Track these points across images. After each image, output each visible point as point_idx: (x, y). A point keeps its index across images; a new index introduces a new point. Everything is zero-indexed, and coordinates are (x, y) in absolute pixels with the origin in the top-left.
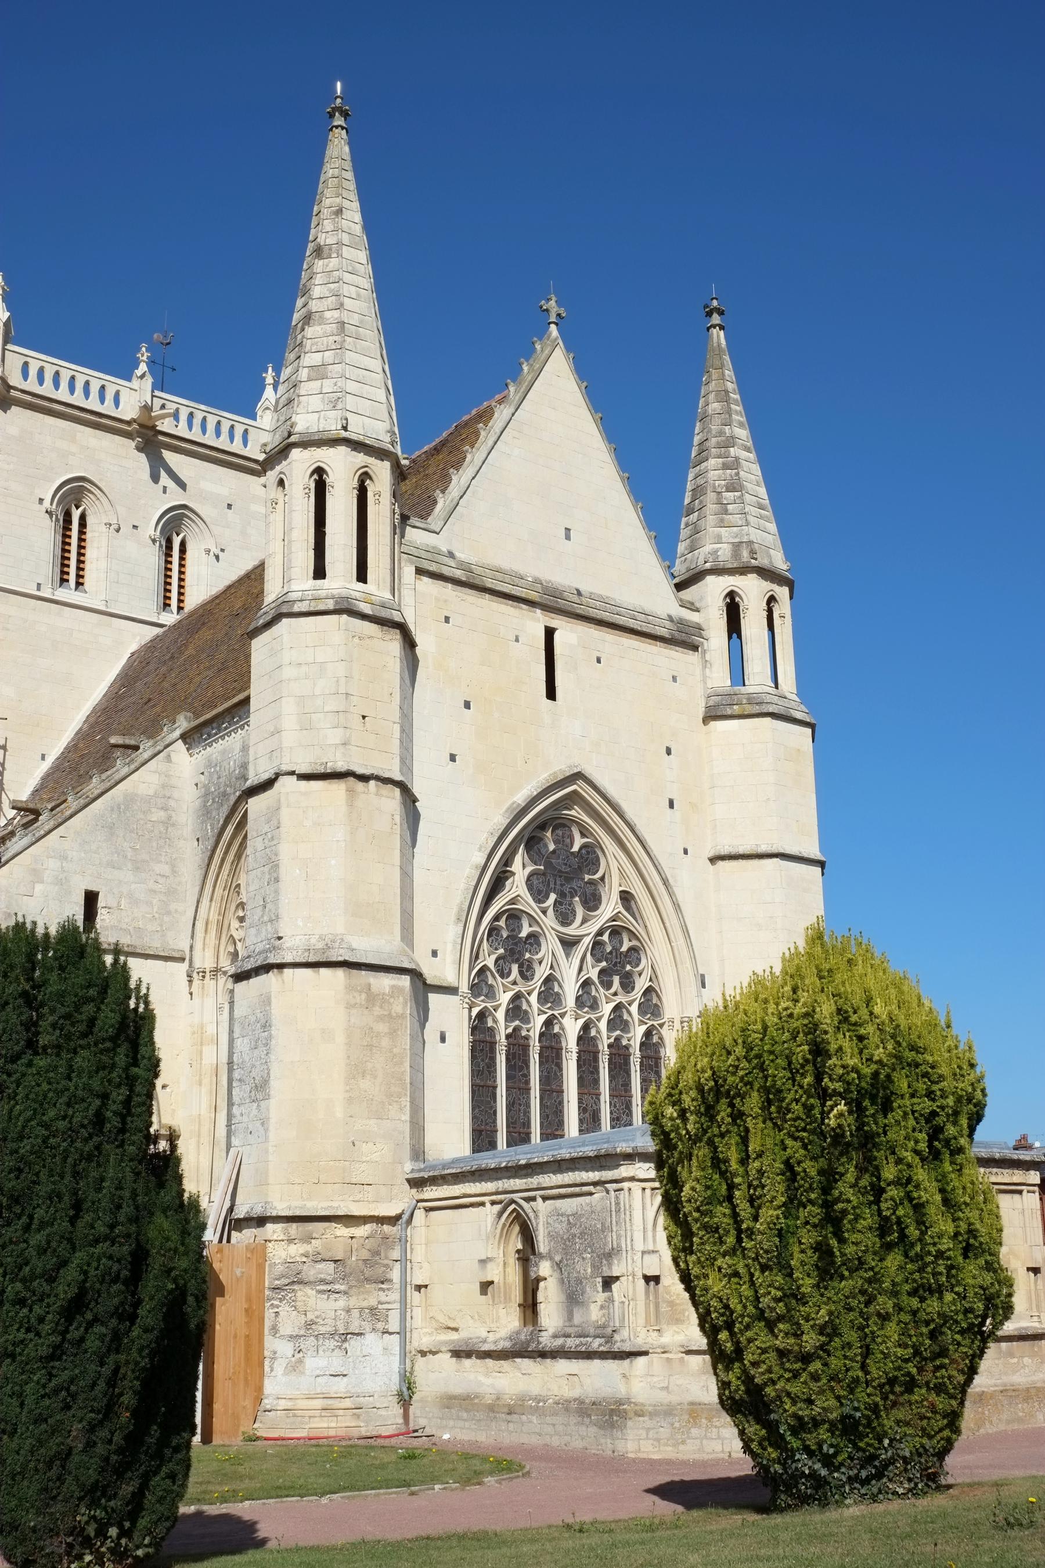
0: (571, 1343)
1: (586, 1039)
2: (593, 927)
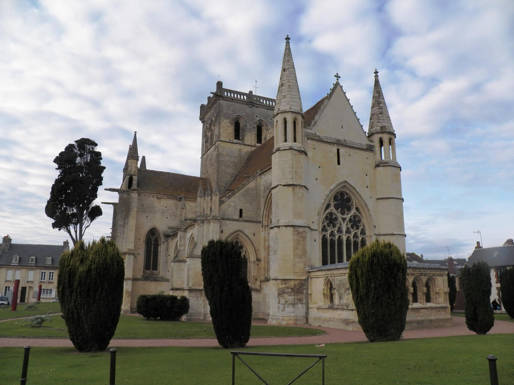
0: (340, 307)
1: (348, 240)
2: (349, 216)
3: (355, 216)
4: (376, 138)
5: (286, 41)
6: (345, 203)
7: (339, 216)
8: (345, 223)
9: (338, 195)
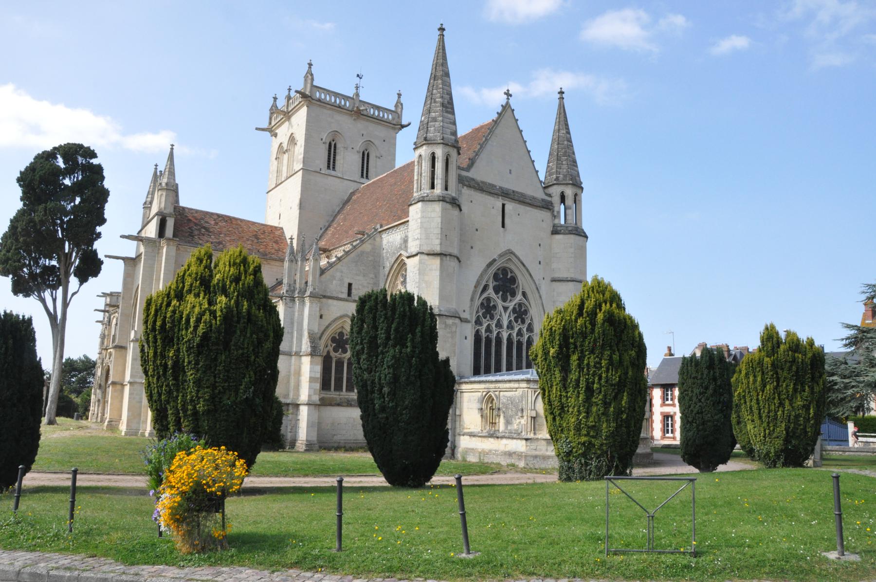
1: (509, 339)
2: (513, 303)
3: (520, 305)
4: (556, 191)
5: (439, 33)
6: (508, 284)
7: (500, 304)
8: (507, 314)
9: (500, 272)
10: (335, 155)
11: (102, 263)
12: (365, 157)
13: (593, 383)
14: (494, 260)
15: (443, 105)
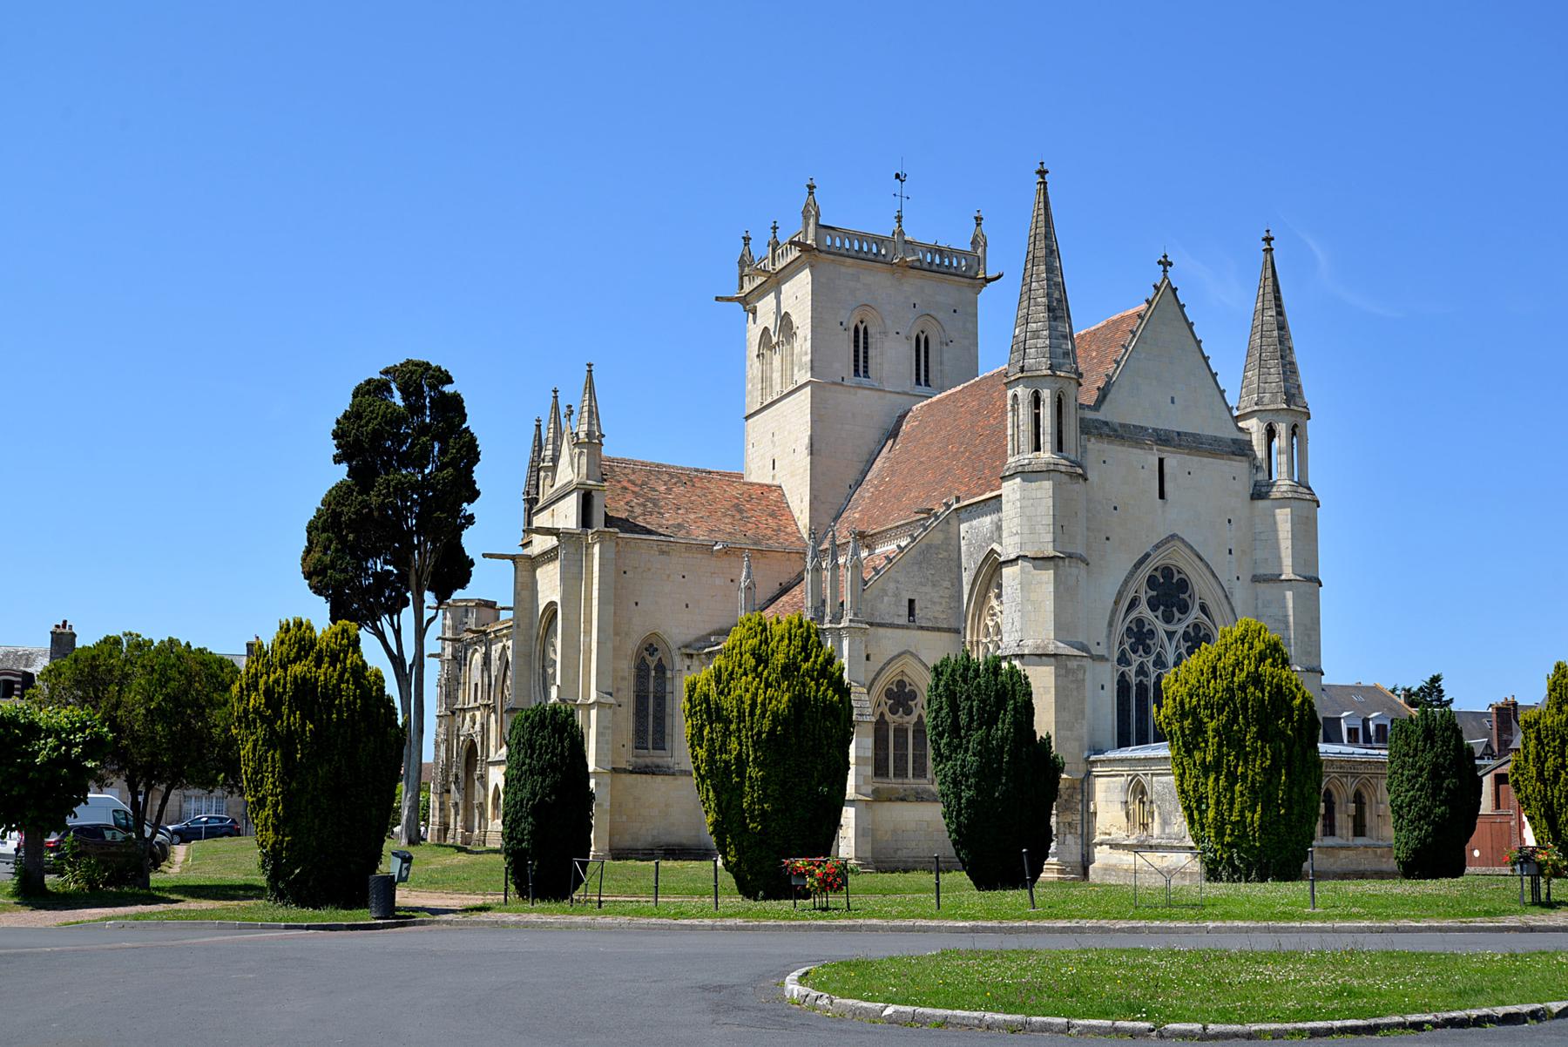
0: (1164, 842)
1: (1140, 685)
3: (1196, 626)
7: (1161, 627)
8: (1174, 643)
9: (1158, 574)
10: (866, 348)
11: (472, 563)
12: (922, 347)
13: (1236, 767)
14: (1147, 555)
15: (1050, 309)
